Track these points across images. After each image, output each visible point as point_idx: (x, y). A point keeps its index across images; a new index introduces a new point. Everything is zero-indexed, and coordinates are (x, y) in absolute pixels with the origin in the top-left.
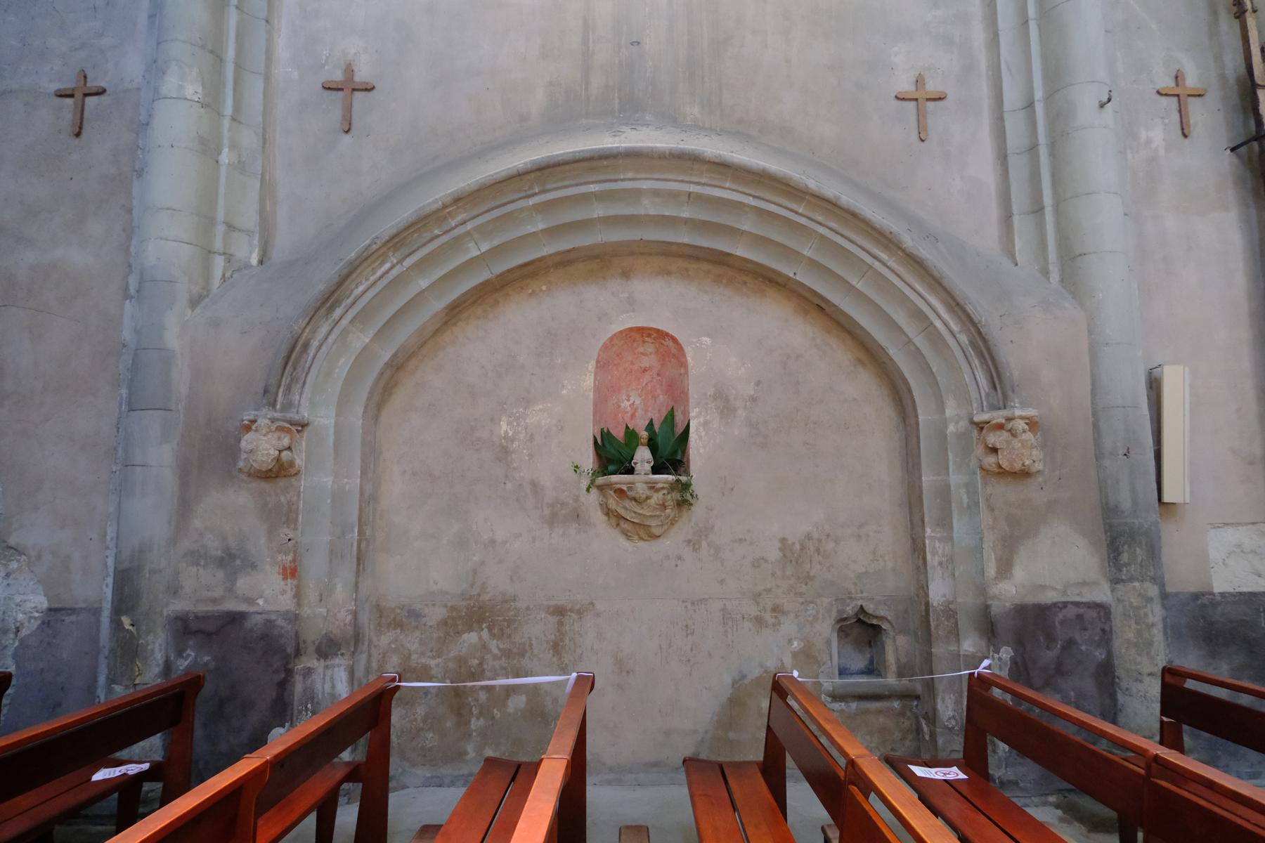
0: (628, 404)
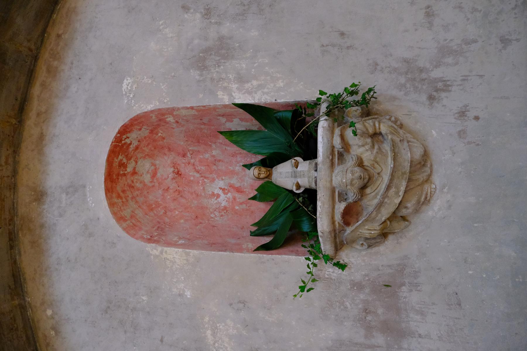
0: (223, 196)
